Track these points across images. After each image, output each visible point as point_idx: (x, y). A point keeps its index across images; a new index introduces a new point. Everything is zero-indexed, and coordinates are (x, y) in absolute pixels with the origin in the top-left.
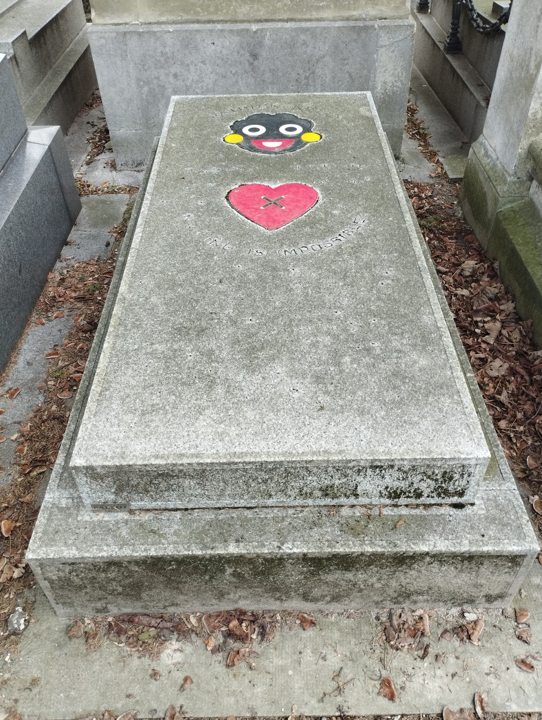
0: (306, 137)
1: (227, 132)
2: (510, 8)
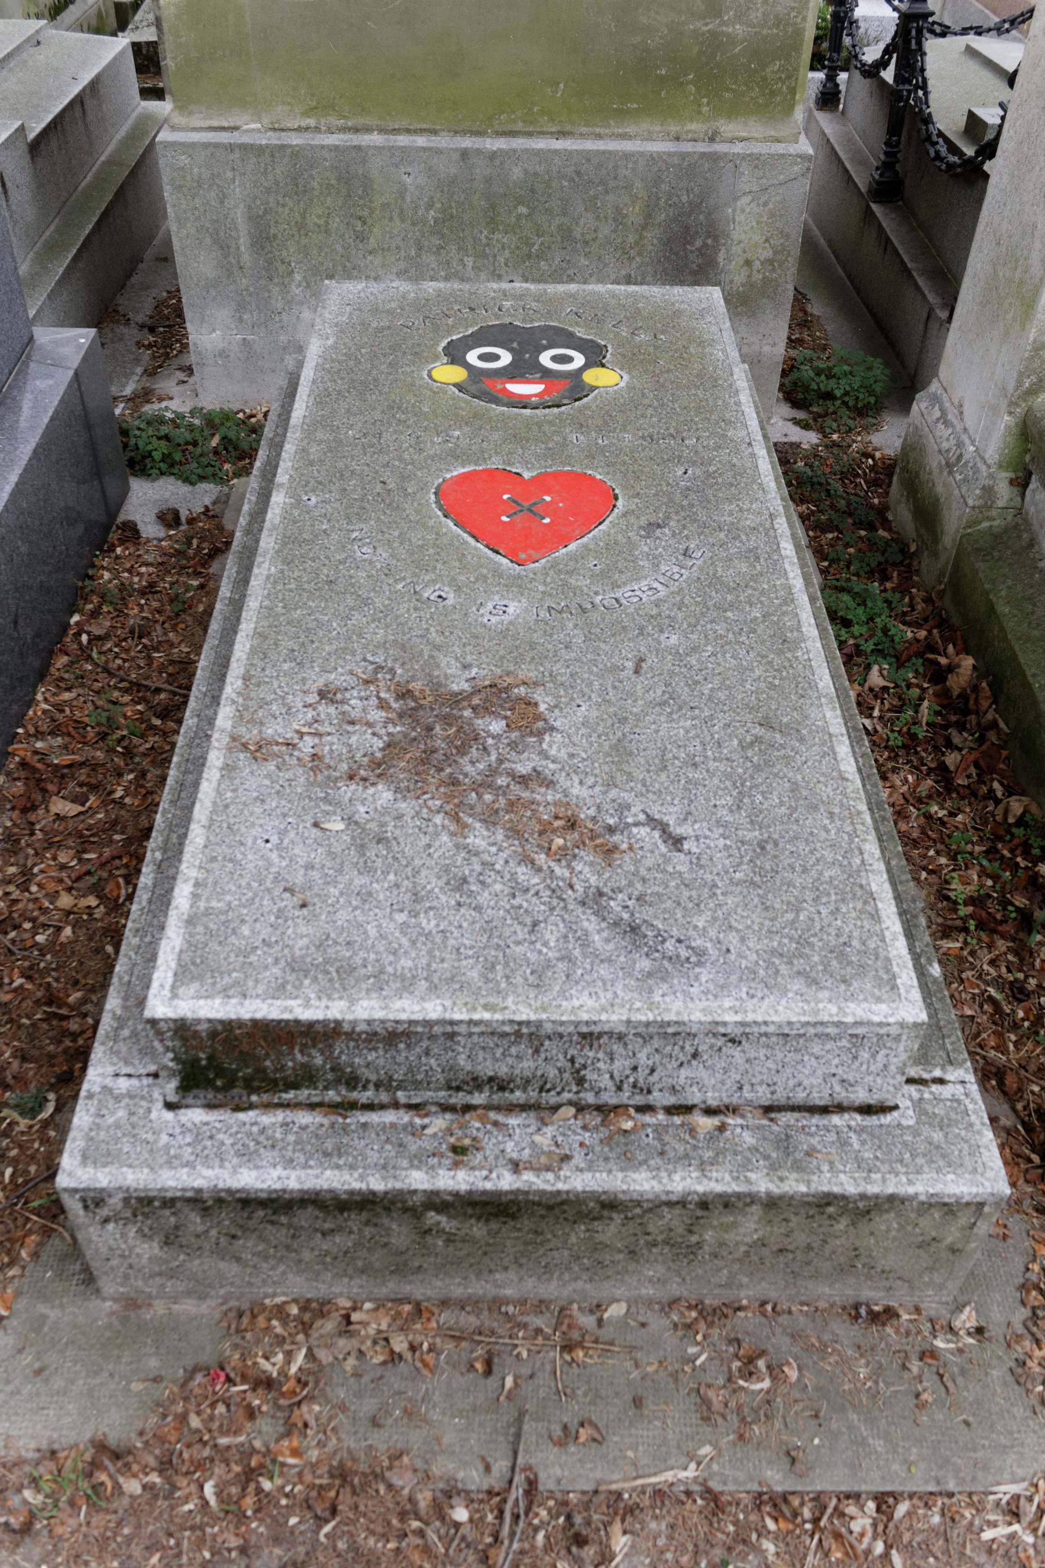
0: (591, 377)
1: (436, 358)
2: (1001, 126)
